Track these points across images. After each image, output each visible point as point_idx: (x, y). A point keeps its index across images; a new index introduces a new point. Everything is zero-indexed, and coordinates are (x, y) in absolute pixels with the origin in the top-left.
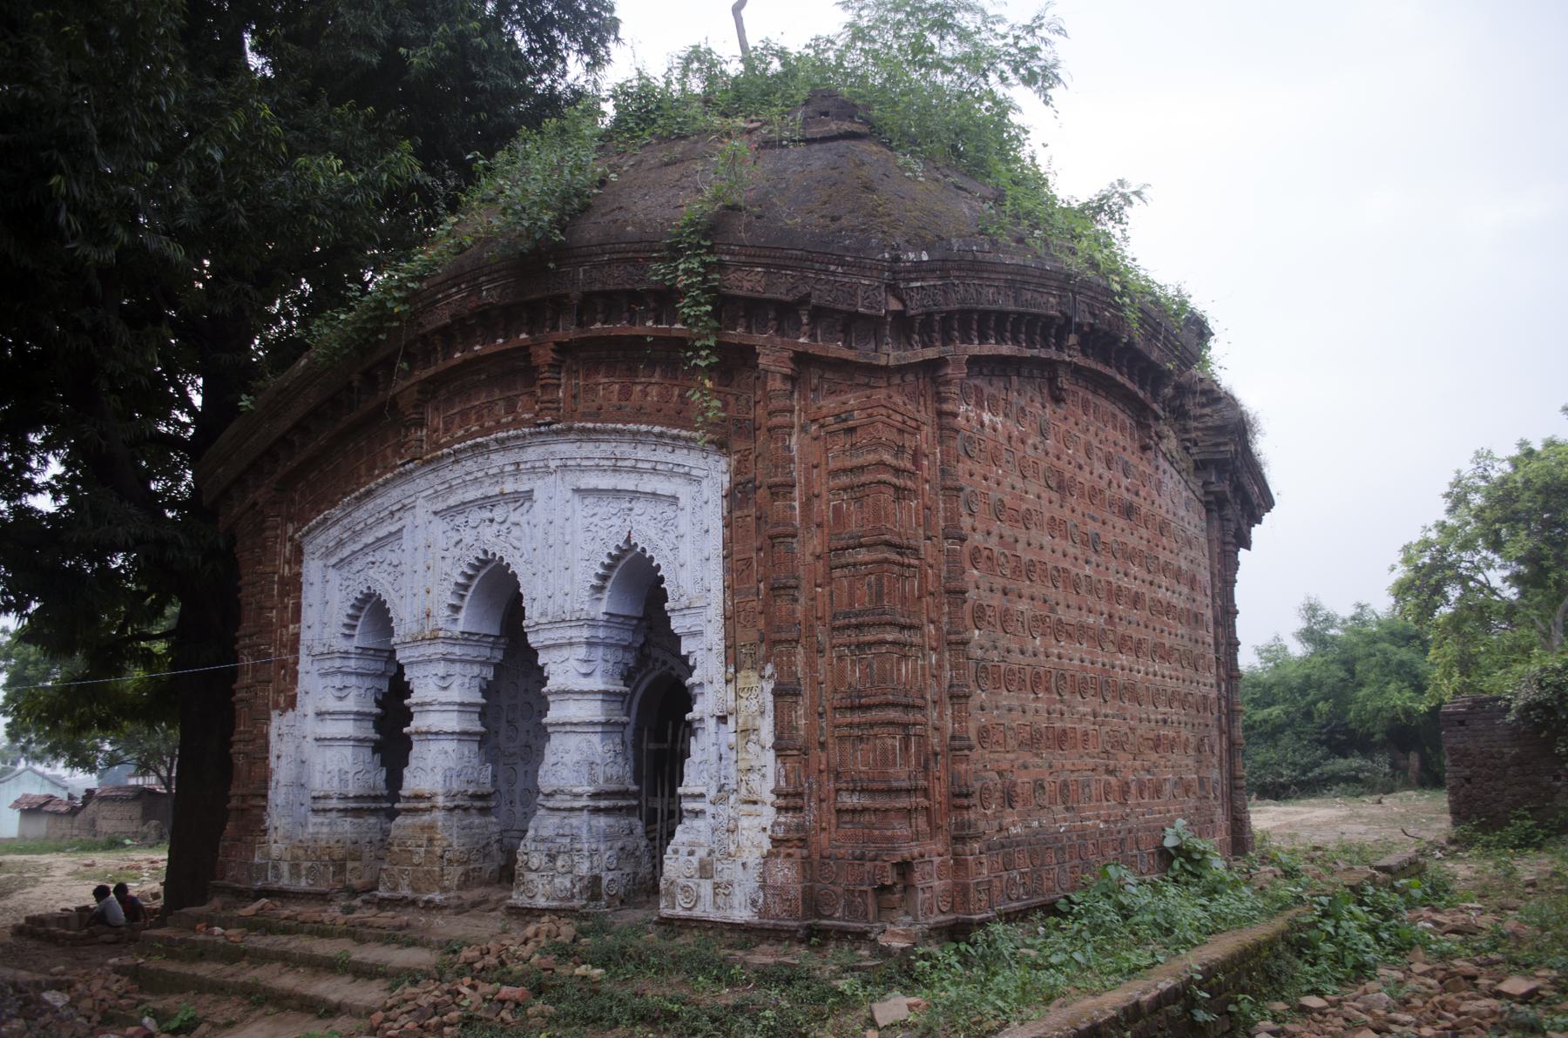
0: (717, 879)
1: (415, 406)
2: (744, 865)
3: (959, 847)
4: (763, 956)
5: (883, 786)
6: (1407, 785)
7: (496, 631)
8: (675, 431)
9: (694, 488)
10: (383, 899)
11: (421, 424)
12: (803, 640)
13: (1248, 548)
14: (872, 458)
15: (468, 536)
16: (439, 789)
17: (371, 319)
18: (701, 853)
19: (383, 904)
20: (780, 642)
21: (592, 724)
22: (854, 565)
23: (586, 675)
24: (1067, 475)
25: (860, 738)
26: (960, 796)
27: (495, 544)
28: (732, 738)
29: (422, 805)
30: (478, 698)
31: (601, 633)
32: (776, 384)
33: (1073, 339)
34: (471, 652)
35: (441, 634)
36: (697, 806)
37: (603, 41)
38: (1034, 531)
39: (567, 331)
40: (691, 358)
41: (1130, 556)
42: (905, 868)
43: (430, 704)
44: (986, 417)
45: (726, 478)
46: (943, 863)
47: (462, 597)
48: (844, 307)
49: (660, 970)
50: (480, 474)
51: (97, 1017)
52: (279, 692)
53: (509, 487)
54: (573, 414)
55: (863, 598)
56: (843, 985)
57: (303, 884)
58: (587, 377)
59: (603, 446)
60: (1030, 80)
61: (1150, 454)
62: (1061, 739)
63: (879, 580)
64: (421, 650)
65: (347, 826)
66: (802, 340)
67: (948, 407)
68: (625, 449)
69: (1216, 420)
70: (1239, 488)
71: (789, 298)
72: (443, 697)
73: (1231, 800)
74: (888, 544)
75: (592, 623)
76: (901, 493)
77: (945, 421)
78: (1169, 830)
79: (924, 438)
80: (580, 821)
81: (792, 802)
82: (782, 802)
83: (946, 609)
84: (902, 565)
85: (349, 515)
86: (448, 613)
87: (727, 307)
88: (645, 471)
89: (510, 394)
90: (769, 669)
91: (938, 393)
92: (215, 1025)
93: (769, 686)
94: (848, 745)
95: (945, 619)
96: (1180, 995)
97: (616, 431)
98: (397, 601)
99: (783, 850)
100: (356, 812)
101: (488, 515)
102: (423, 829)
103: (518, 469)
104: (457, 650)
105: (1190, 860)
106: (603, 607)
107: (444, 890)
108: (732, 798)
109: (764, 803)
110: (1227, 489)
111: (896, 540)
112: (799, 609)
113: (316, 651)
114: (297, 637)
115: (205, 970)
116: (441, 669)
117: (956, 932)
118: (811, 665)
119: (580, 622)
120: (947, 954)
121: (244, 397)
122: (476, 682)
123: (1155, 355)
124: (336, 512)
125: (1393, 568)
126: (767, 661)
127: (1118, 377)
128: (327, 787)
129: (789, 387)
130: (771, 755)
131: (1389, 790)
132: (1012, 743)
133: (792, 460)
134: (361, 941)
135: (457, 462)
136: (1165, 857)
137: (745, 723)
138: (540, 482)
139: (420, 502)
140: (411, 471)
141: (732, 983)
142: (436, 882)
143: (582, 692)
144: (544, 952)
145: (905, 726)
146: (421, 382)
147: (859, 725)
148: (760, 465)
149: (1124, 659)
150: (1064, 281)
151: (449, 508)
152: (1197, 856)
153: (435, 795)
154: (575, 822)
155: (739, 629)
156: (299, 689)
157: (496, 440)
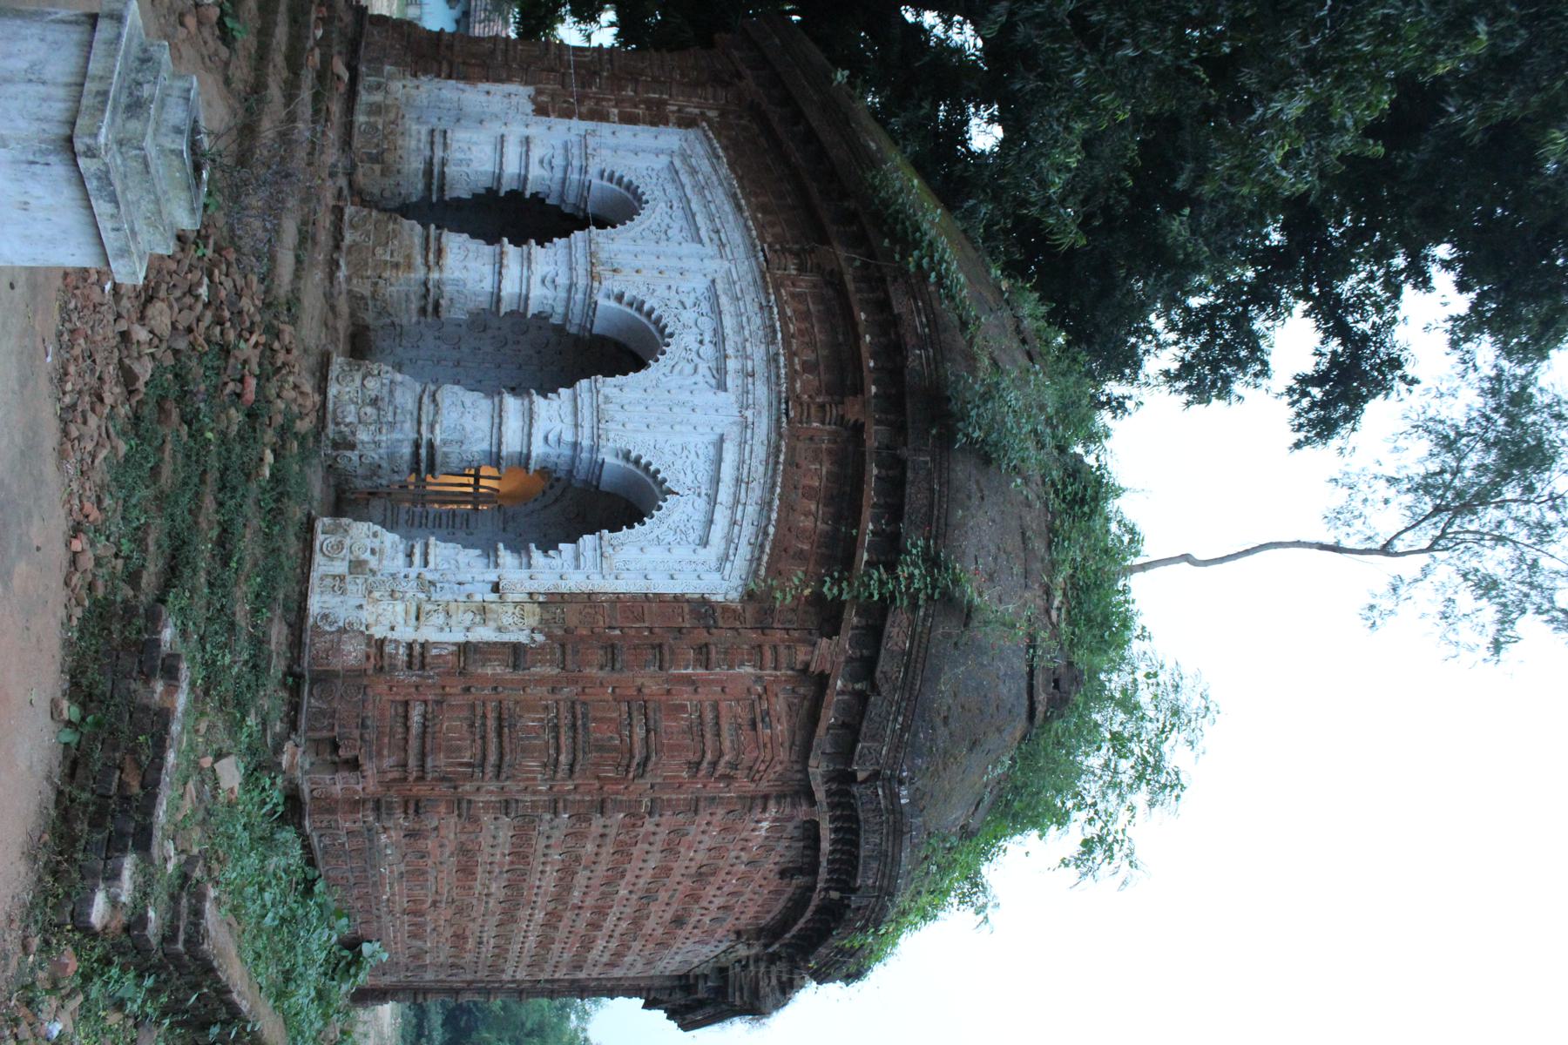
0: (349, 578)
1: (819, 266)
2: (361, 607)
3: (370, 805)
4: (278, 634)
5: (428, 748)
7: (596, 330)
8: (767, 550)
9: (714, 564)
11: (801, 269)
12: (564, 674)
13: (644, 1007)
14: (727, 744)
15: (688, 316)
16: (447, 274)
17: (905, 230)
18: (373, 562)
19: (338, 212)
20: (564, 653)
21: (500, 444)
22: (630, 725)
23: (546, 439)
24: (712, 879)
25: (472, 725)
26: (415, 807)
27: (678, 345)
28: (478, 598)
29: (431, 257)
31: (585, 455)
32: (801, 655)
33: (835, 895)
34: (577, 309)
35: (596, 284)
36: (417, 558)
37: (1189, 389)
38: (659, 855)
39: (874, 436)
40: (832, 577)
41: (636, 922)
42: (354, 765)
43: (529, 267)
44: (765, 824)
45: (720, 598)
46: (356, 792)
47: (630, 304)
48: (864, 729)
49: (268, 536)
50: (747, 333)
52: (553, 96)
53: (732, 365)
54: (794, 436)
55: (601, 732)
56: (251, 721)
57: (361, 118)
58: (830, 452)
59: (761, 469)
60: (1088, 844)
61: (733, 937)
62: (466, 871)
63: (615, 748)
64: (582, 260)
65: (416, 164)
66: (839, 683)
67: (772, 805)
68: (756, 492)
70: (701, 1004)
71: (878, 674)
72: (537, 276)
73: (404, 989)
74: (647, 758)
75: (595, 448)
77: (759, 802)
78: (377, 945)
79: (744, 784)
80: (407, 432)
81: (416, 661)
82: (417, 648)
83: (588, 798)
84: (628, 766)
85: (721, 184)
86: (616, 290)
87: (876, 617)
88: (734, 513)
89: (822, 368)
90: (539, 638)
91: (785, 796)
92: (227, 64)
93: (523, 638)
94: (466, 714)
95: (578, 797)
96: (234, 1013)
97: (774, 485)
98: (632, 234)
99: (373, 651)
100: (428, 172)
101: (707, 339)
102: (409, 257)
103: (748, 375)
104: (579, 296)
105: (349, 965)
106: (610, 460)
107: (349, 279)
108: (422, 596)
109: (417, 629)
110: (700, 996)
111: (650, 766)
112: (592, 671)
113: (591, 141)
114: (602, 117)
115: (281, 33)
116: (562, 280)
117: (293, 808)
118: (540, 681)
119: (597, 437)
120: (277, 796)
121: (846, 73)
122: (548, 309)
123: (822, 950)
124: (724, 170)
126: (549, 636)
127: (803, 920)
128: (455, 146)
129: (798, 667)
130: (460, 637)
132: (464, 838)
133: (731, 667)
135: (761, 307)
136: (352, 944)
137: (492, 611)
138: (733, 398)
139: (726, 264)
140: (757, 258)
141: (256, 611)
142: (358, 269)
143: (530, 435)
144: (287, 413)
145: (482, 765)
146: (841, 274)
147: (484, 724)
148: (729, 634)
149: (540, 916)
150: (888, 892)
151: (717, 297)
152: (352, 971)
153: (441, 270)
154: (407, 426)
155: (581, 606)
156: (553, 120)
157: (777, 354)
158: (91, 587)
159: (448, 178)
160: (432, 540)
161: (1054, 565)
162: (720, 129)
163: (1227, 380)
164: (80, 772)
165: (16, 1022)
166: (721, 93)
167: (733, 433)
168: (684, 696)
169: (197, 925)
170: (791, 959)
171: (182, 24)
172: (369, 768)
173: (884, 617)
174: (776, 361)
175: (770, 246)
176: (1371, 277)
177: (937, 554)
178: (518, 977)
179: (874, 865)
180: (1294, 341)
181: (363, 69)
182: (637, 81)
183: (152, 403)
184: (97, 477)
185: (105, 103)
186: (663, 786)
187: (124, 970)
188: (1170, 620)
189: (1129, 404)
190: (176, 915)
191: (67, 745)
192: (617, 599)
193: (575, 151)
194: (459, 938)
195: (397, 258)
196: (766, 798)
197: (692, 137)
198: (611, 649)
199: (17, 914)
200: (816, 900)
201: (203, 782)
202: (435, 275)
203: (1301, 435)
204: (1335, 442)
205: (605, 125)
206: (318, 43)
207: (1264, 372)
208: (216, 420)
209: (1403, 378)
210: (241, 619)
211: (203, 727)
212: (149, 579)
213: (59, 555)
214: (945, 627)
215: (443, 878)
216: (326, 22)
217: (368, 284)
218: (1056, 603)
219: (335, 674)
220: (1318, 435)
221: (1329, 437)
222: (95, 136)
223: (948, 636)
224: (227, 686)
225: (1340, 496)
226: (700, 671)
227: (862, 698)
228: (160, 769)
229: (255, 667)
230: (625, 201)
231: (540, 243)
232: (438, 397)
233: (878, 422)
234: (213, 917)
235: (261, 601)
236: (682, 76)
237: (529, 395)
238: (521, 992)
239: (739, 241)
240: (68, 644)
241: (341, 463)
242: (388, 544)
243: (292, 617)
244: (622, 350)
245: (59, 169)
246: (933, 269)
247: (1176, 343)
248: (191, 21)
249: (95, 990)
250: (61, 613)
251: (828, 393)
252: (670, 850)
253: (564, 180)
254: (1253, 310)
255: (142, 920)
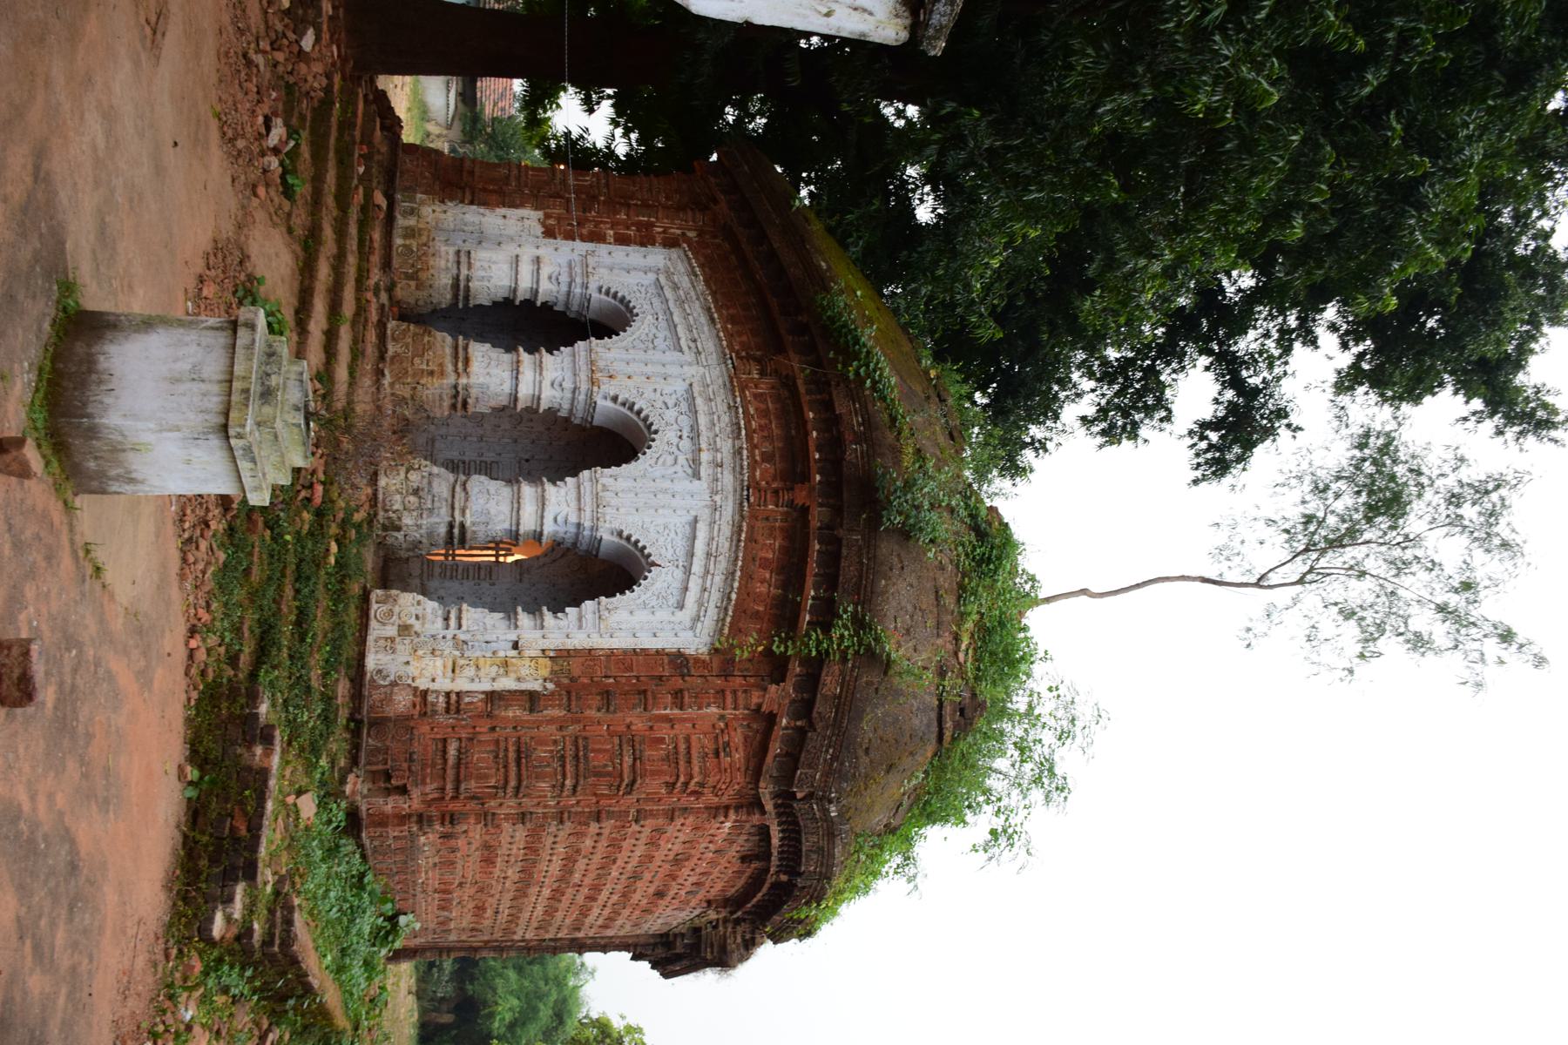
2: (408, 663)
3: (414, 819)
4: (343, 689)
6: (423, 1012)
7: (595, 423)
9: (688, 624)
10: (385, 326)
11: (762, 373)
13: (633, 958)
14: (696, 769)
15: (670, 415)
16: (473, 380)
17: (847, 342)
18: (417, 626)
19: (381, 325)
20: (569, 699)
21: (518, 524)
23: (555, 520)
25: (497, 757)
26: (453, 819)
28: (501, 654)
29: (460, 365)
30: (544, 406)
33: (784, 878)
36: (453, 622)
37: (1103, 433)
39: (817, 517)
42: (403, 790)
44: (728, 824)
47: (624, 404)
49: (334, 613)
51: (292, 80)
52: (559, 219)
55: (598, 760)
56: (323, 762)
57: (398, 241)
59: (727, 545)
62: (488, 861)
63: (609, 774)
64: (584, 368)
65: (445, 280)
68: (723, 564)
69: (731, 946)
70: (679, 957)
71: (815, 715)
72: (548, 379)
74: (633, 782)
75: (594, 528)
76: (671, 786)
78: (411, 916)
79: (710, 798)
82: (454, 697)
87: (814, 668)
88: (704, 582)
90: (550, 686)
92: (289, 215)
93: (536, 686)
94: (492, 748)
96: (308, 990)
97: (736, 559)
99: (418, 700)
100: (456, 285)
101: (685, 434)
102: (441, 365)
104: (582, 397)
105: (388, 933)
107: (392, 385)
112: (591, 713)
113: (591, 260)
116: (568, 385)
117: (353, 824)
118: (551, 721)
124: (701, 286)
125: (623, 1017)
126: (557, 684)
130: (487, 686)
131: (420, 995)
132: (487, 838)
134: (354, 323)
135: (729, 407)
136: (393, 919)
138: (705, 485)
141: (325, 675)
142: (398, 378)
143: (542, 517)
149: (546, 892)
156: (560, 242)
158: (203, 673)
159: (472, 291)
160: (465, 606)
161: (963, 616)
162: (697, 248)
163: (1135, 425)
164: (201, 820)
165: (164, 1012)
166: (699, 216)
167: (705, 515)
168: (663, 731)
169: (288, 931)
170: (753, 922)
171: (256, 195)
172: (416, 793)
173: (821, 669)
174: (740, 453)
175: (737, 353)
176: (1267, 335)
177: (864, 616)
178: (528, 936)
179: (814, 856)
180: (1195, 391)
181: (399, 196)
182: (629, 206)
183: (243, 515)
184: (207, 589)
185: (247, 399)
186: (647, 800)
187: (232, 967)
188: (1061, 644)
189: (1049, 445)
190: (273, 926)
191: (189, 799)
192: (611, 653)
193: (578, 270)
194: (480, 909)
195: (432, 367)
196: (727, 808)
197: (674, 256)
198: (606, 695)
199: (160, 932)
200: (770, 879)
201: (288, 815)
202: (463, 381)
203: (1199, 473)
204: (1228, 480)
205: (603, 246)
206: (361, 179)
207: (1168, 419)
208: (292, 522)
209: (1289, 426)
210: (315, 683)
211: (288, 773)
212: (245, 659)
213: (181, 654)
214: (869, 677)
215: (468, 864)
216: (367, 158)
217: (408, 388)
218: (963, 647)
219: (388, 719)
220: (1214, 473)
221: (1222, 475)
222: (243, 426)
223: (869, 684)
224: (305, 739)
225: (1220, 538)
226: (676, 711)
227: (802, 732)
228: (262, 816)
229: (326, 718)
230: (616, 311)
231: (550, 352)
232: (468, 486)
233: (821, 505)
234: (299, 919)
235: (329, 667)
236: (667, 198)
237: (542, 484)
238: (529, 949)
239: (712, 349)
240: (189, 721)
241: (390, 541)
242: (429, 610)
243: (352, 672)
244: (612, 443)
245: (215, 442)
246: (868, 375)
247: (1093, 391)
248: (261, 191)
249: (211, 982)
250: (184, 697)
251: (782, 479)
252: (653, 843)
253: (569, 293)
254: (1159, 365)
255: (249, 931)
